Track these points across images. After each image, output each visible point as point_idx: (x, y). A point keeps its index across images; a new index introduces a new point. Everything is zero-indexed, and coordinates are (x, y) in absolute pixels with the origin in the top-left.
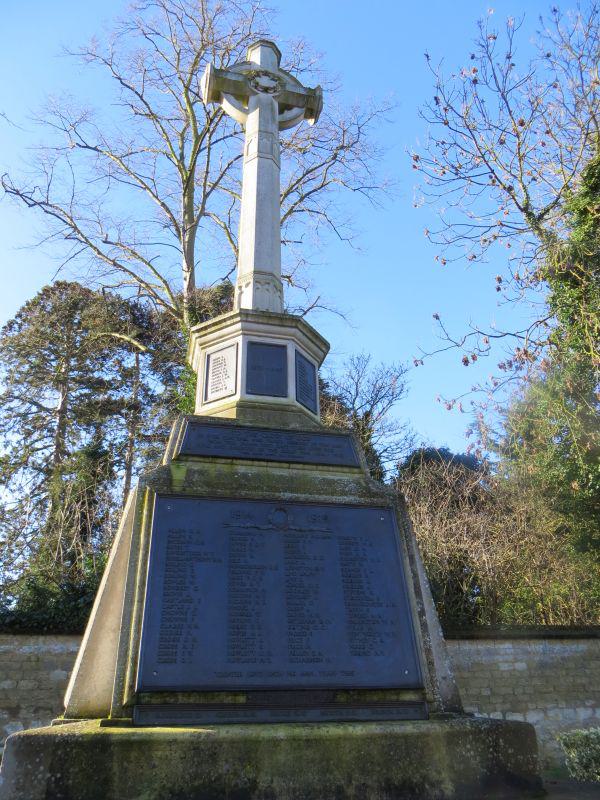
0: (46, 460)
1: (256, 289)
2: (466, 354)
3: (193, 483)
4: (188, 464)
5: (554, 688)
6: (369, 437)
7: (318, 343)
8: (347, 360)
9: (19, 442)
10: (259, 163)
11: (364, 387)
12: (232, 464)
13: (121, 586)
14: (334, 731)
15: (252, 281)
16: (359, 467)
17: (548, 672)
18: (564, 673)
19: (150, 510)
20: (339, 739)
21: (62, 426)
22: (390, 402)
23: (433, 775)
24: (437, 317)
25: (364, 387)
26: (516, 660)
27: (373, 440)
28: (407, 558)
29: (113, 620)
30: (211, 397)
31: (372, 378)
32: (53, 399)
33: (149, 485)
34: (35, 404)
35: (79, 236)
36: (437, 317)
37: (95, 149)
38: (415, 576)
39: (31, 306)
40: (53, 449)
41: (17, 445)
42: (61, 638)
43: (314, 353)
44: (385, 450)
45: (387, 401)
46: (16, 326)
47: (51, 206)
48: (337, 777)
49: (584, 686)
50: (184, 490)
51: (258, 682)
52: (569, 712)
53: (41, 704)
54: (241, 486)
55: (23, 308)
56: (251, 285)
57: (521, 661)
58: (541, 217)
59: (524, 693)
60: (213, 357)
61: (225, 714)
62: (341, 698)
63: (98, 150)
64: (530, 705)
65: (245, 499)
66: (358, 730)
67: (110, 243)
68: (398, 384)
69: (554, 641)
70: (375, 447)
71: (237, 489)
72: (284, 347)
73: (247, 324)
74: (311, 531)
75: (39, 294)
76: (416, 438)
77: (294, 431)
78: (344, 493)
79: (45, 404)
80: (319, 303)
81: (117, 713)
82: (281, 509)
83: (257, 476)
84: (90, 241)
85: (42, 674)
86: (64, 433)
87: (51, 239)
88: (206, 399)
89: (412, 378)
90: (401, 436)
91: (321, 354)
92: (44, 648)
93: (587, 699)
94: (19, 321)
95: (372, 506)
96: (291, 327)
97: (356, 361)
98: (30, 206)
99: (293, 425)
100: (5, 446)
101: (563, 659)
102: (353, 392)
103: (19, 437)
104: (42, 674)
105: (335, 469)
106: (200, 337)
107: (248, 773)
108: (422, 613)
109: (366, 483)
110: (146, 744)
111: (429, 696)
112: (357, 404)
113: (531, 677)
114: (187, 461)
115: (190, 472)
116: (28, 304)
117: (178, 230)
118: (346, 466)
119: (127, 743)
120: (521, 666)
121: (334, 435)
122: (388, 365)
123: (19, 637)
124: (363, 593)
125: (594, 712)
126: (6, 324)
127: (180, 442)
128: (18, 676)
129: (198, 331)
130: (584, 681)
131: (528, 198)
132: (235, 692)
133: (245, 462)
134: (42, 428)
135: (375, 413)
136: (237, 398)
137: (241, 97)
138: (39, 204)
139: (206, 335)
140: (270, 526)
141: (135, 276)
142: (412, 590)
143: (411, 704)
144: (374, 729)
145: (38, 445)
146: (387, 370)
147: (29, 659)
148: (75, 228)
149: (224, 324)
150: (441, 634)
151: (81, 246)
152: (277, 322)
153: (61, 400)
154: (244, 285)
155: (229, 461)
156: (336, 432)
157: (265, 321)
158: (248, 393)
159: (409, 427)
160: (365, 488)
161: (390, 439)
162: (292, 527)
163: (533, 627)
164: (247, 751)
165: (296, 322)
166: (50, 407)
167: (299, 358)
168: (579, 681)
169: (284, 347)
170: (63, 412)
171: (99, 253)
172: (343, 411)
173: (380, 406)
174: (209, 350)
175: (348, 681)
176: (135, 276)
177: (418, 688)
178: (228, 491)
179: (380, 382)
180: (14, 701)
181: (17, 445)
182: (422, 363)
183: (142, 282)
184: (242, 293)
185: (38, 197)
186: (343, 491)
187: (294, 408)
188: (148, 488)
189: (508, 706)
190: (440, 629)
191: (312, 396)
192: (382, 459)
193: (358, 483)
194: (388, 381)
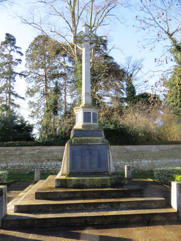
1: (85, 97)
5: (165, 155)
10: (85, 64)
13: (66, 158)
14: (94, 178)
17: (164, 152)
18: (168, 152)
20: (95, 179)
23: (108, 183)
26: (156, 149)
29: (66, 163)
32: (42, 72)
37: (45, 2)
38: (109, 155)
40: (44, 87)
42: (56, 147)
44: (136, 85)
46: (29, 51)
48: (95, 184)
49: (173, 155)
51: (85, 172)
52: (168, 160)
53: (53, 159)
55: (30, 45)
58: (172, 34)
61: (81, 176)
62: (97, 173)
63: (46, 3)
64: (158, 159)
65: (83, 145)
66: (98, 178)
67: (52, 32)
69: (166, 145)
72: (90, 112)
77: (92, 131)
78: (99, 142)
79: (40, 74)
83: (85, 140)
85: (53, 153)
92: (52, 149)
93: (173, 157)
94: (30, 49)
95: (103, 145)
97: (128, 58)
99: (92, 129)
101: (168, 149)
104: (53, 153)
107: (83, 183)
108: (110, 161)
110: (71, 180)
111: (109, 173)
113: (160, 153)
115: (75, 140)
116: (31, 44)
119: (69, 180)
120: (157, 150)
123: (47, 147)
125: (174, 160)
126: (26, 51)
128: (48, 154)
130: (173, 153)
131: (168, 29)
132: (82, 173)
135: (134, 74)
137: (81, 42)
142: (108, 158)
143: (106, 174)
144: (100, 178)
147: (50, 151)
163: (91, 185)
164: (83, 180)
168: (171, 154)
169: (90, 112)
170: (45, 76)
173: (135, 72)
175: (97, 171)
177: (108, 172)
180: (48, 159)
185: (30, 21)
189: (153, 159)
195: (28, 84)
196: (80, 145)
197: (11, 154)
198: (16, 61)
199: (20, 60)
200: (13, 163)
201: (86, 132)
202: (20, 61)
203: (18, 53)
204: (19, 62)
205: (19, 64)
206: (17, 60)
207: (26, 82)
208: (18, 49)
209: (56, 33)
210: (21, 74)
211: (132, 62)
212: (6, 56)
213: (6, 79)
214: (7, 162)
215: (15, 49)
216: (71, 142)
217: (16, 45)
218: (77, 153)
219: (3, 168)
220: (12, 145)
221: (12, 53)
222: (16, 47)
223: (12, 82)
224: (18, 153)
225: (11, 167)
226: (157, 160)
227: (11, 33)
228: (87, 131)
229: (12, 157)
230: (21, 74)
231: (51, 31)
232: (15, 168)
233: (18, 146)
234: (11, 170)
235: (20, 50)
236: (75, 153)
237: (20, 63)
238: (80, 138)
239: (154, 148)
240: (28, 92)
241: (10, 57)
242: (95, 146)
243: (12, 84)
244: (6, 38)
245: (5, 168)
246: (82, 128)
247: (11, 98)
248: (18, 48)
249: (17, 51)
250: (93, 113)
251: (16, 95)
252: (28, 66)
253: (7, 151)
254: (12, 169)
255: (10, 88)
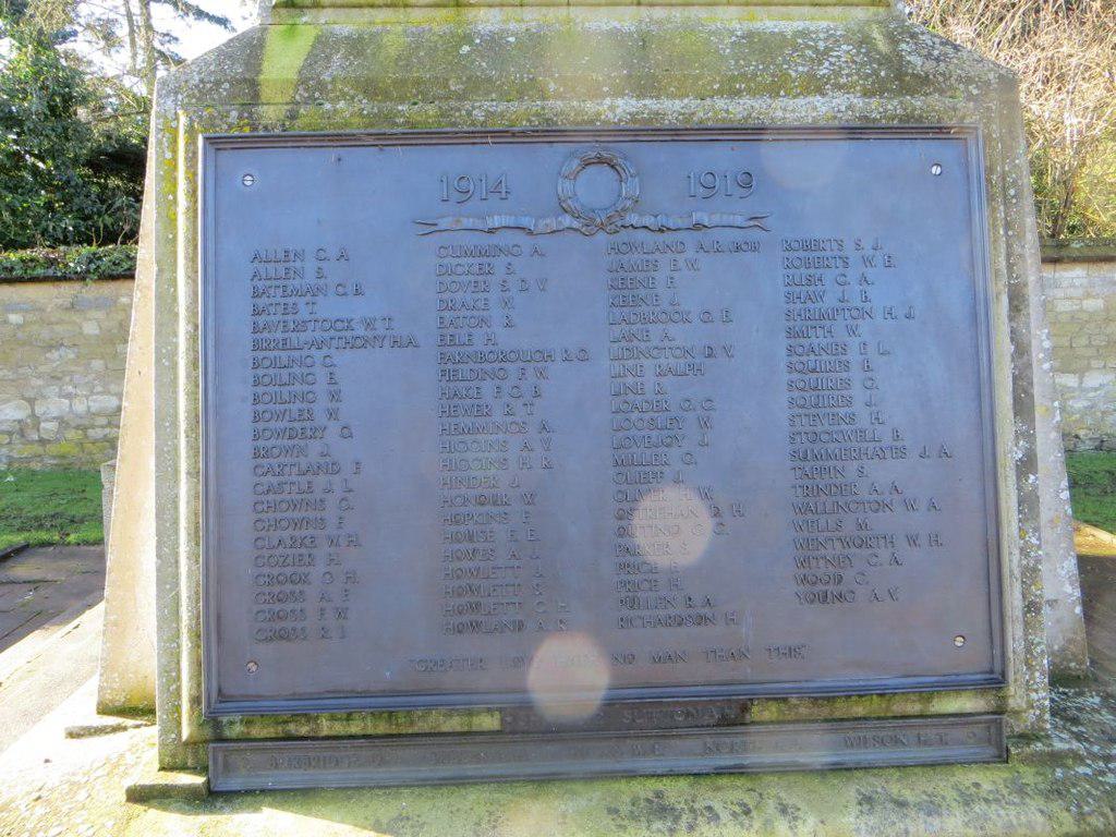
3: (321, 87)
19: (192, 180)
26: (1088, 296)
28: (1005, 299)
33: (185, 108)
38: (1021, 350)
50: (293, 116)
54: (476, 86)
57: (1097, 296)
59: (1089, 345)
64: (1094, 363)
71: (461, 97)
74: (698, 227)
78: (815, 86)
81: (173, 756)
82: (600, 161)
108: (1027, 465)
109: (893, 40)
124: (852, 418)
140: (567, 221)
142: (1005, 399)
150: (1065, 495)
160: (885, 60)
162: (634, 219)
178: (432, 110)
186: (812, 76)
190: (1065, 483)
193: (865, 41)
196: (415, 137)
197: (45, 334)
200: (69, 396)
214: (30, 394)
218: (357, 309)
219: (10, 433)
220: (40, 271)
224: (90, 329)
225: (62, 422)
226: (1081, 373)
229: (55, 354)
232: (91, 432)
233: (81, 277)
234: (64, 448)
236: (328, 307)
239: (1072, 286)
242: (723, 157)
245: (22, 433)
253: (14, 318)
254: (71, 434)
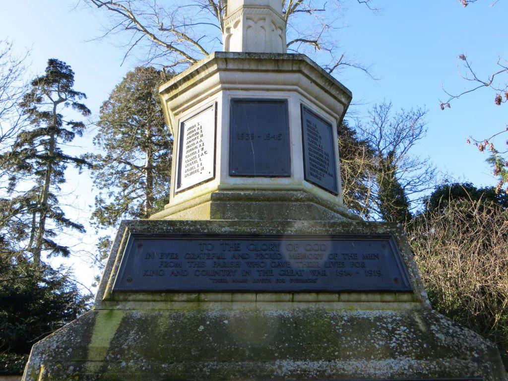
0: (141, 205)
1: (246, 28)
2: (499, 92)
3: (122, 352)
4: (129, 305)
6: (394, 173)
7: (333, 92)
8: (371, 109)
9: (120, 193)
11: (387, 130)
12: (199, 300)
15: (241, 18)
16: (411, 292)
21: (150, 179)
22: (411, 142)
24: (463, 58)
25: (387, 130)
27: (398, 176)
30: (185, 183)
31: (394, 122)
34: (129, 163)
35: (138, 26)
36: (463, 58)
39: (119, 89)
40: (145, 198)
41: (118, 195)
43: (328, 106)
44: (408, 184)
45: (408, 142)
47: (115, 4)
56: (240, 25)
60: (187, 125)
68: (417, 125)
70: (400, 181)
72: (284, 103)
73: (228, 74)
75: (124, 79)
76: (436, 171)
80: (343, 61)
84: (147, 29)
86: (151, 185)
87: (113, 31)
88: (179, 186)
89: (433, 120)
90: (423, 170)
91: (340, 107)
96: (292, 71)
97: (379, 109)
98: (99, 6)
100: (110, 196)
102: (378, 136)
103: (121, 189)
105: (371, 297)
106: (172, 99)
112: (382, 146)
114: (126, 300)
117: (216, 10)
118: (389, 292)
121: (365, 236)
122: (407, 110)
126: (102, 105)
127: (117, 268)
129: (168, 91)
133: (219, 296)
134: (135, 182)
135: (398, 152)
136: (214, 185)
138: (105, 4)
139: (176, 96)
141: (184, 54)
145: (133, 195)
146: (406, 114)
148: (134, 20)
149: (197, 78)
151: (140, 34)
152: (271, 67)
153: (147, 159)
154: (231, 25)
155: (194, 296)
156: (367, 231)
157: (253, 67)
158: (231, 175)
159: (429, 162)
161: (412, 174)
165: (299, 62)
166: (140, 165)
167: (307, 116)
169: (284, 103)
170: (149, 169)
171: (155, 38)
172: (370, 152)
173: (402, 146)
174: (183, 116)
176: (184, 54)
179: (401, 125)
181: (118, 195)
182: (449, 106)
183: (190, 58)
184: (230, 36)
187: (300, 195)
188: (43, 370)
191: (330, 170)
192: (406, 191)
193: (412, 324)
194: (409, 124)
195: (101, 191)
198: (69, 128)
199: (81, 125)
201: (244, 245)
202: (79, 128)
203: (77, 109)
204: (76, 130)
205: (77, 136)
206: (71, 126)
207: (95, 185)
208: (76, 97)
209: (182, 58)
210: (80, 162)
211: (391, 119)
212: (45, 115)
213: (39, 177)
215: (70, 99)
216: (82, 352)
217: (75, 88)
221: (61, 109)
222: (73, 93)
223: (54, 182)
227: (60, 58)
228: (254, 236)
230: (80, 162)
231: (162, 29)
235: (82, 101)
237: (80, 133)
238: (182, 306)
240: (98, 214)
241: (58, 119)
243: (52, 189)
244: (48, 70)
246: (213, 213)
247: (47, 227)
248: (77, 93)
249: (75, 104)
250: (303, 108)
251: (60, 218)
252: (103, 142)
255: (46, 199)
